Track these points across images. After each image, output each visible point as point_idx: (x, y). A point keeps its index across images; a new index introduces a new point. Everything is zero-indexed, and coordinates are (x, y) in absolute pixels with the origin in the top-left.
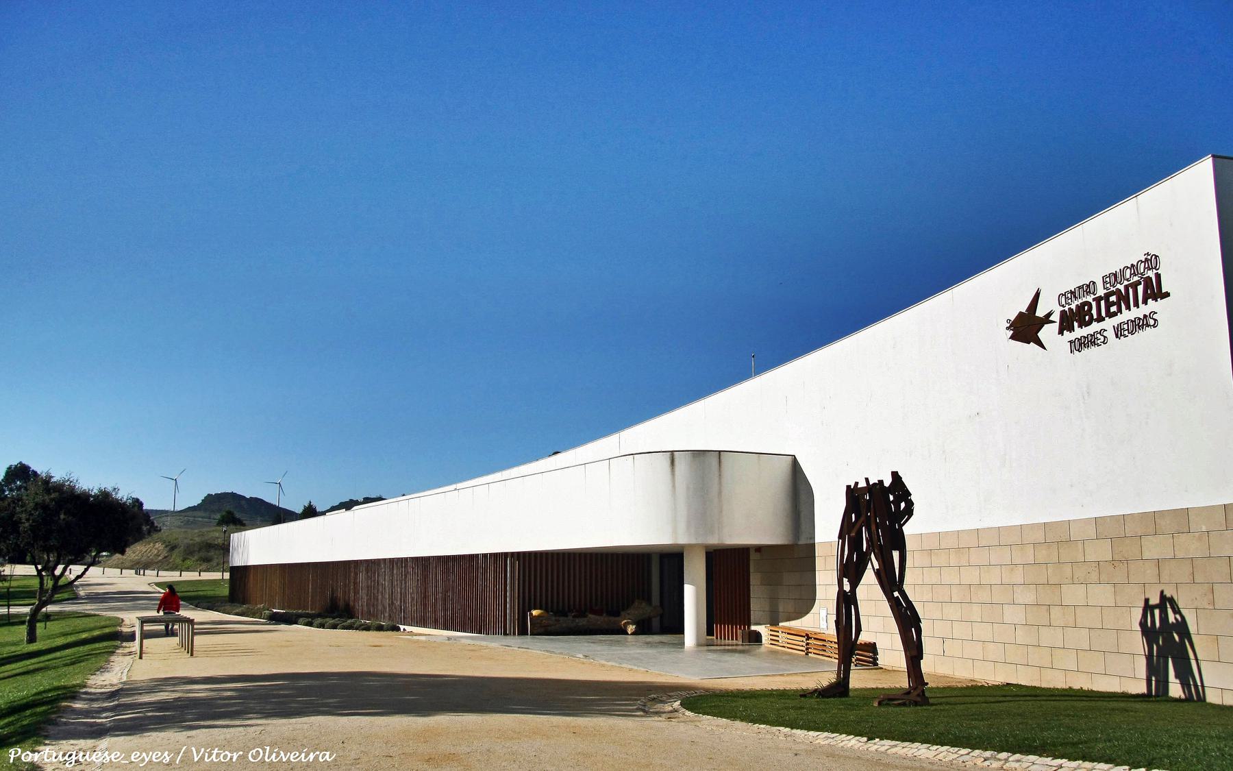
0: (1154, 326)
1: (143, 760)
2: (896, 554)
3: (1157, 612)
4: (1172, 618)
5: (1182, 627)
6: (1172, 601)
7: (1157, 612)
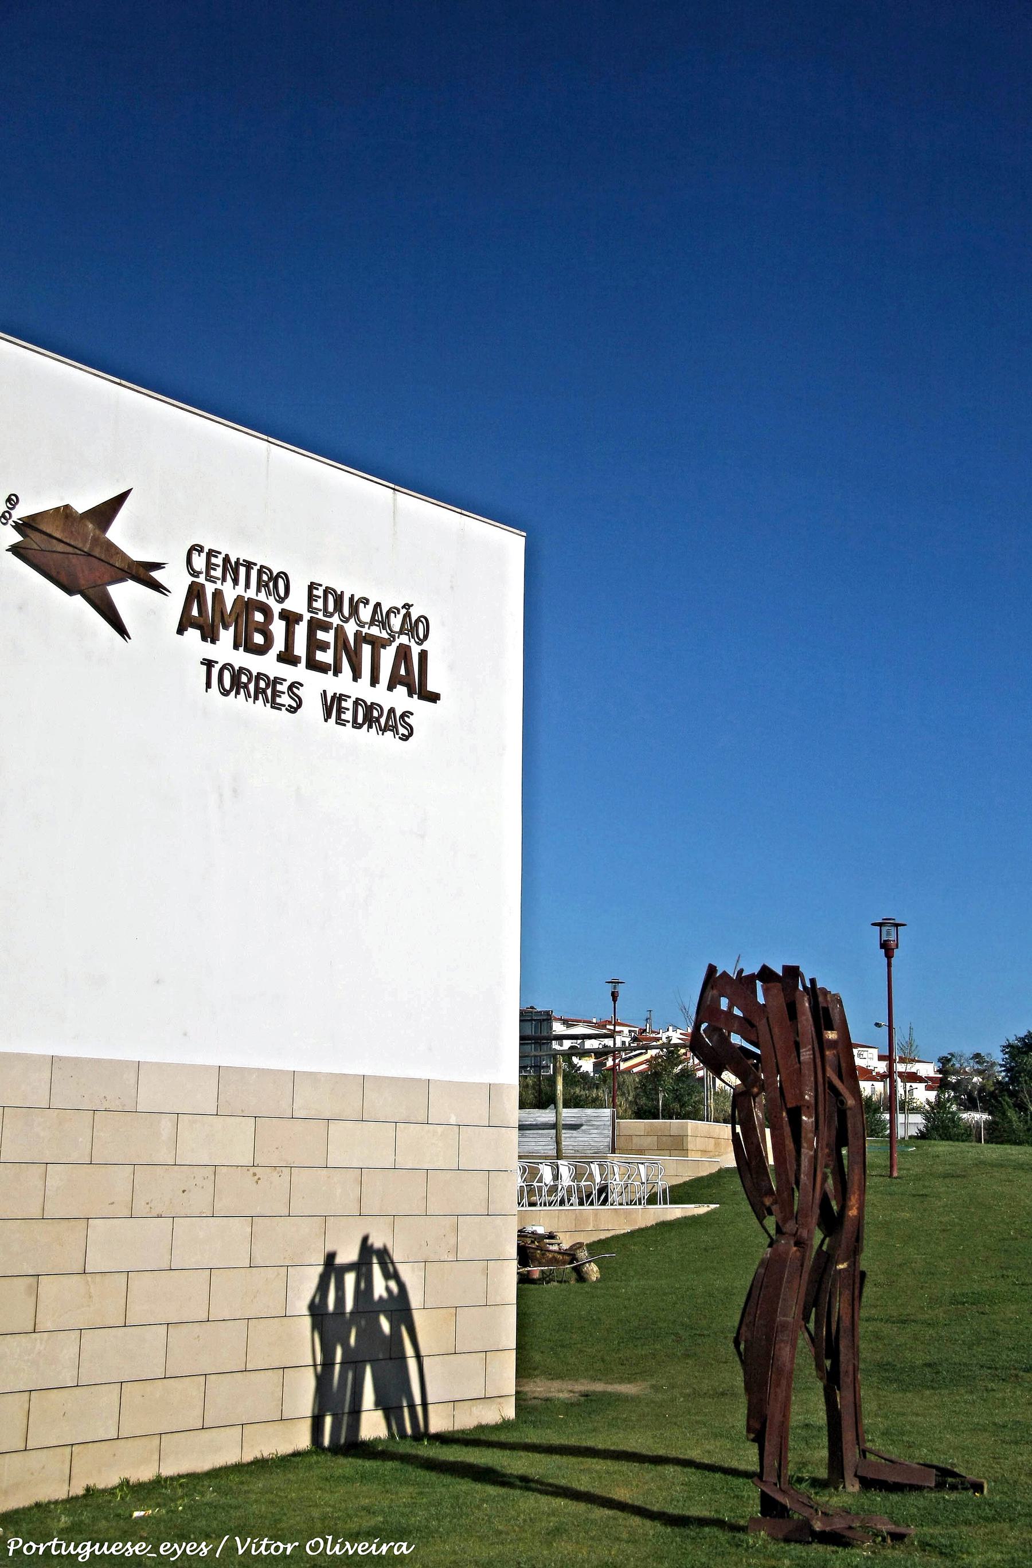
0: (293, 710)
1: (175, 1553)
2: (824, 1248)
3: (350, 1279)
4: (380, 1287)
5: (399, 1307)
6: (384, 1255)
7: (350, 1279)
